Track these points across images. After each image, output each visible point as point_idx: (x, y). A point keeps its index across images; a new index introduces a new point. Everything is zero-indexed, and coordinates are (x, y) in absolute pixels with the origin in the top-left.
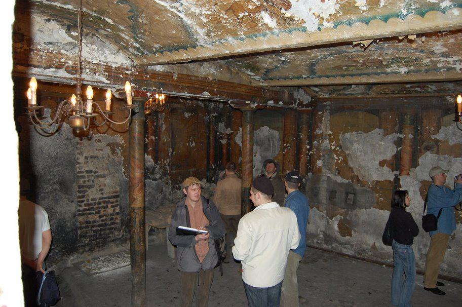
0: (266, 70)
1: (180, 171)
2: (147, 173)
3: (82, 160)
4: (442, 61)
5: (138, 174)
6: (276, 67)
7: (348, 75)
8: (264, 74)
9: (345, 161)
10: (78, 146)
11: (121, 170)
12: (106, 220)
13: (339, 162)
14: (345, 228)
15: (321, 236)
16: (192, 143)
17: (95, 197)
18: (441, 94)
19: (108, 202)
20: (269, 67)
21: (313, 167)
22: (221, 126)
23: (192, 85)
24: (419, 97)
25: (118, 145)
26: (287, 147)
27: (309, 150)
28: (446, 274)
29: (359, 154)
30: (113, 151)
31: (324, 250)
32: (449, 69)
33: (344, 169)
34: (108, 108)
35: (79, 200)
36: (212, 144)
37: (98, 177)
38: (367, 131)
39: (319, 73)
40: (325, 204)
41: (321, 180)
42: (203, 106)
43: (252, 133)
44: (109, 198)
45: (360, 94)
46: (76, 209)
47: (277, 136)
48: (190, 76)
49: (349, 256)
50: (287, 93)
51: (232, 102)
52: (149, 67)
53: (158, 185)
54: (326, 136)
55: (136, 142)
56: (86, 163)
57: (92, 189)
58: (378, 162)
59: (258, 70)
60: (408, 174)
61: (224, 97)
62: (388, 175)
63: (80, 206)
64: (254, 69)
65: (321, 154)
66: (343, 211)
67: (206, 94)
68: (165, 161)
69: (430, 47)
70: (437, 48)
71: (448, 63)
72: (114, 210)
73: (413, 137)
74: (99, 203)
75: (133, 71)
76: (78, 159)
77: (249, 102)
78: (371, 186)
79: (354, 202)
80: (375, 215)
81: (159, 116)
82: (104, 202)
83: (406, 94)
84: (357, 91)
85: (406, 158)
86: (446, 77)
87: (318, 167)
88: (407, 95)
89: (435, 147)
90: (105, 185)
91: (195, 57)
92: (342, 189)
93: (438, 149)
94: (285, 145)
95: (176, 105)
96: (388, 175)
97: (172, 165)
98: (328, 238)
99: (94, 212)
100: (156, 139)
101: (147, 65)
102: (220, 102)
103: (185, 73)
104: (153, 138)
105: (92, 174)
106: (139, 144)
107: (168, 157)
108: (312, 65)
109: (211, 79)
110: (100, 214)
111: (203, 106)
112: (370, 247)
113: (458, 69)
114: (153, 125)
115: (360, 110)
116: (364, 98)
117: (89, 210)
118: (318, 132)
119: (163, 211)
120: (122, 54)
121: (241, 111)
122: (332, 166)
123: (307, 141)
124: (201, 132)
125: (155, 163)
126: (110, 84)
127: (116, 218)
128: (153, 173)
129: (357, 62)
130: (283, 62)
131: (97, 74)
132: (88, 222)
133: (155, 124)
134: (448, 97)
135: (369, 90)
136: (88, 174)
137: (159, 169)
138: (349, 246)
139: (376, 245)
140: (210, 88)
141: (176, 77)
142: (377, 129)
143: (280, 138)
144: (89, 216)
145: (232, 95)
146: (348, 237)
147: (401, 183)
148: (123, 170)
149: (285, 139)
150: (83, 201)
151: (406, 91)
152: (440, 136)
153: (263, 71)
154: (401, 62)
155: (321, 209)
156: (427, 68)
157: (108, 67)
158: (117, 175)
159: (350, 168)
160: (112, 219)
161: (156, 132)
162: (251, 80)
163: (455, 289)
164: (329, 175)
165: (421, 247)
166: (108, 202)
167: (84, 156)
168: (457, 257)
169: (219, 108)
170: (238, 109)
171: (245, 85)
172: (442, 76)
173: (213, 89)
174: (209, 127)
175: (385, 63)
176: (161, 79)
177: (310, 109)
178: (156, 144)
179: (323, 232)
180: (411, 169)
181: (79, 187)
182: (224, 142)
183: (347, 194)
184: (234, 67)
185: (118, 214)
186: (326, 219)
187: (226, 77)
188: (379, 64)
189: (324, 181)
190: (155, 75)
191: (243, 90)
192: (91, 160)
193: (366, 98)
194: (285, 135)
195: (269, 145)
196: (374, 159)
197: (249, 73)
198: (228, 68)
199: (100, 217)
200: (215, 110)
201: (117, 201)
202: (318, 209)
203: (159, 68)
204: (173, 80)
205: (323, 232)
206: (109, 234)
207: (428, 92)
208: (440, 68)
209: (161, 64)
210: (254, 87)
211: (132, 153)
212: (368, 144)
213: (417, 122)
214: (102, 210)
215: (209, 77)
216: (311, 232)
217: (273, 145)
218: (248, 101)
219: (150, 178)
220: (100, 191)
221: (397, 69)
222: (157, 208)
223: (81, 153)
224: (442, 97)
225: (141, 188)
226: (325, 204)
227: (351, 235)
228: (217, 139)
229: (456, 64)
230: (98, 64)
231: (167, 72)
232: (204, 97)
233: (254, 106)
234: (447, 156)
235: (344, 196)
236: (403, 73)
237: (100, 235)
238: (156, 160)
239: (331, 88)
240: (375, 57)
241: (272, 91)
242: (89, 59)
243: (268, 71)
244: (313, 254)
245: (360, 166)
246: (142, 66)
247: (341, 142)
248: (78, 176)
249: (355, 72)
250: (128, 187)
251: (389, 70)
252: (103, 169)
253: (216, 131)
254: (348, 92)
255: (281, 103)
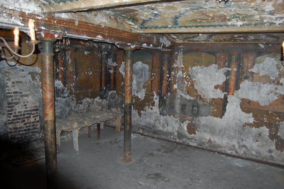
0: (143, 21)
1: (82, 91)
2: (57, 92)
3: (10, 84)
4: (267, 17)
5: (49, 95)
6: (150, 19)
7: (200, 26)
8: (141, 24)
9: (192, 85)
10: (7, 74)
11: (40, 91)
12: (29, 126)
13: (188, 86)
14: (192, 129)
15: (176, 134)
16: (90, 72)
17: (21, 110)
18: (256, 42)
19: (31, 114)
20: (145, 19)
21: (171, 89)
22: (110, 61)
23: (89, 30)
24: (242, 43)
25: (37, 73)
26: (154, 75)
27: (169, 78)
28: (254, 158)
29: (201, 81)
30: (33, 78)
31: (178, 143)
32: (271, 24)
33: (191, 90)
34: (16, 43)
35: (8, 113)
36: (103, 73)
37: (22, 96)
38: (207, 65)
39: (180, 24)
40: (179, 114)
41: (176, 98)
42: (97, 47)
43: (131, 66)
44: (31, 111)
45: (204, 41)
46: (7, 119)
47: (147, 68)
48: (87, 23)
49: (194, 147)
50: (155, 38)
51: (118, 44)
52: (56, 14)
53: (66, 101)
54: (180, 68)
55: (47, 72)
56: (13, 86)
57: (18, 105)
58: (213, 86)
59: (137, 21)
60: (233, 94)
61: (113, 40)
62: (220, 95)
63: (10, 117)
64: (134, 20)
65: (177, 80)
66: (190, 118)
67: (99, 38)
68: (71, 85)
69: (263, 7)
70: (268, 7)
71: (271, 19)
72: (35, 119)
73: (237, 70)
74: (24, 115)
75: (43, 17)
76: (7, 83)
77: (130, 44)
78: (209, 102)
79: (198, 112)
80: (211, 120)
81: (67, 53)
82: (27, 114)
83: (233, 41)
84: (202, 38)
85: (232, 83)
86: (268, 30)
87: (174, 89)
88: (234, 42)
89: (251, 76)
90: (28, 102)
91: (91, 6)
92: (190, 104)
93: (252, 78)
94: (153, 74)
95: (78, 46)
96: (220, 95)
97: (76, 87)
98: (180, 135)
99: (21, 121)
100: (64, 70)
101: (54, 13)
102: (109, 43)
103: (84, 20)
104: (62, 68)
105: (18, 94)
106: (50, 73)
107: (73, 82)
108: (176, 18)
109: (103, 26)
110: (25, 122)
111: (97, 47)
112: (207, 141)
113: (277, 24)
114: (62, 60)
115: (203, 52)
116: (206, 44)
117: (17, 119)
118: (175, 66)
119: (70, 119)
120: (33, 3)
121: (124, 51)
122: (184, 88)
123: (167, 72)
124: (96, 65)
125: (64, 86)
126: (24, 26)
127: (37, 125)
128: (62, 93)
129: (208, 16)
130: (156, 14)
131: (13, 18)
132: (16, 128)
133: (64, 59)
134: (260, 45)
135: (210, 38)
136: (15, 95)
137: (67, 90)
138: (194, 140)
139: (211, 139)
140: (102, 33)
141: (77, 23)
142: (214, 65)
143: (149, 69)
144: (17, 124)
145: (118, 39)
146: (193, 135)
147: (228, 100)
148: (41, 91)
149: (153, 70)
150: (11, 114)
151: (234, 40)
152: (254, 70)
153: (141, 22)
154: (239, 17)
155: (176, 116)
156: (256, 22)
157: (22, 13)
158: (36, 94)
159: (195, 90)
160: (34, 125)
161: (65, 65)
162: (132, 28)
163: (261, 167)
164: (182, 95)
165: (240, 141)
166: (31, 114)
167: (12, 81)
168: (262, 147)
169: (108, 48)
170: (122, 49)
171: (128, 32)
172: (265, 28)
173: (104, 33)
174: (101, 61)
175: (228, 18)
176: (65, 25)
177: (170, 50)
178: (64, 73)
179: (177, 131)
180: (235, 91)
181: (9, 104)
182: (112, 71)
183: (193, 107)
184: (120, 18)
185: (38, 122)
186: (179, 122)
187: (114, 25)
188: (224, 18)
189: (178, 98)
190: (60, 21)
191: (126, 35)
192: (17, 84)
193: (207, 43)
194: (153, 67)
195: (142, 74)
196: (211, 84)
197: (130, 23)
198: (116, 19)
199: (25, 124)
200: (106, 49)
201: (37, 113)
202: (174, 117)
203: (64, 16)
204: (75, 26)
205: (177, 131)
206: (32, 136)
207: (248, 40)
208: (265, 23)
209: (65, 12)
210: (134, 33)
211: (44, 80)
212: (208, 74)
213: (239, 60)
214: (26, 120)
215: (102, 25)
216: (169, 131)
217: (144, 74)
218: (130, 43)
219: (61, 97)
220: (24, 106)
221: (235, 23)
222: (66, 117)
223: (9, 80)
224: (256, 44)
225: (52, 106)
226: (179, 114)
227: (195, 134)
228: (107, 69)
229: (277, 20)
230: (14, 10)
231: (70, 19)
232: (98, 40)
233: (133, 47)
234: (258, 83)
235: (191, 108)
236: (239, 26)
237: (25, 136)
238: (65, 84)
239: (185, 36)
240: (222, 13)
241: (146, 37)
242: (6, 5)
243: (144, 22)
244: (171, 146)
245: (202, 89)
246: (50, 13)
247: (190, 73)
248: (7, 96)
249: (205, 24)
250: (43, 102)
251: (229, 23)
252: (26, 91)
253: (106, 64)
254: (195, 39)
255: (151, 45)
